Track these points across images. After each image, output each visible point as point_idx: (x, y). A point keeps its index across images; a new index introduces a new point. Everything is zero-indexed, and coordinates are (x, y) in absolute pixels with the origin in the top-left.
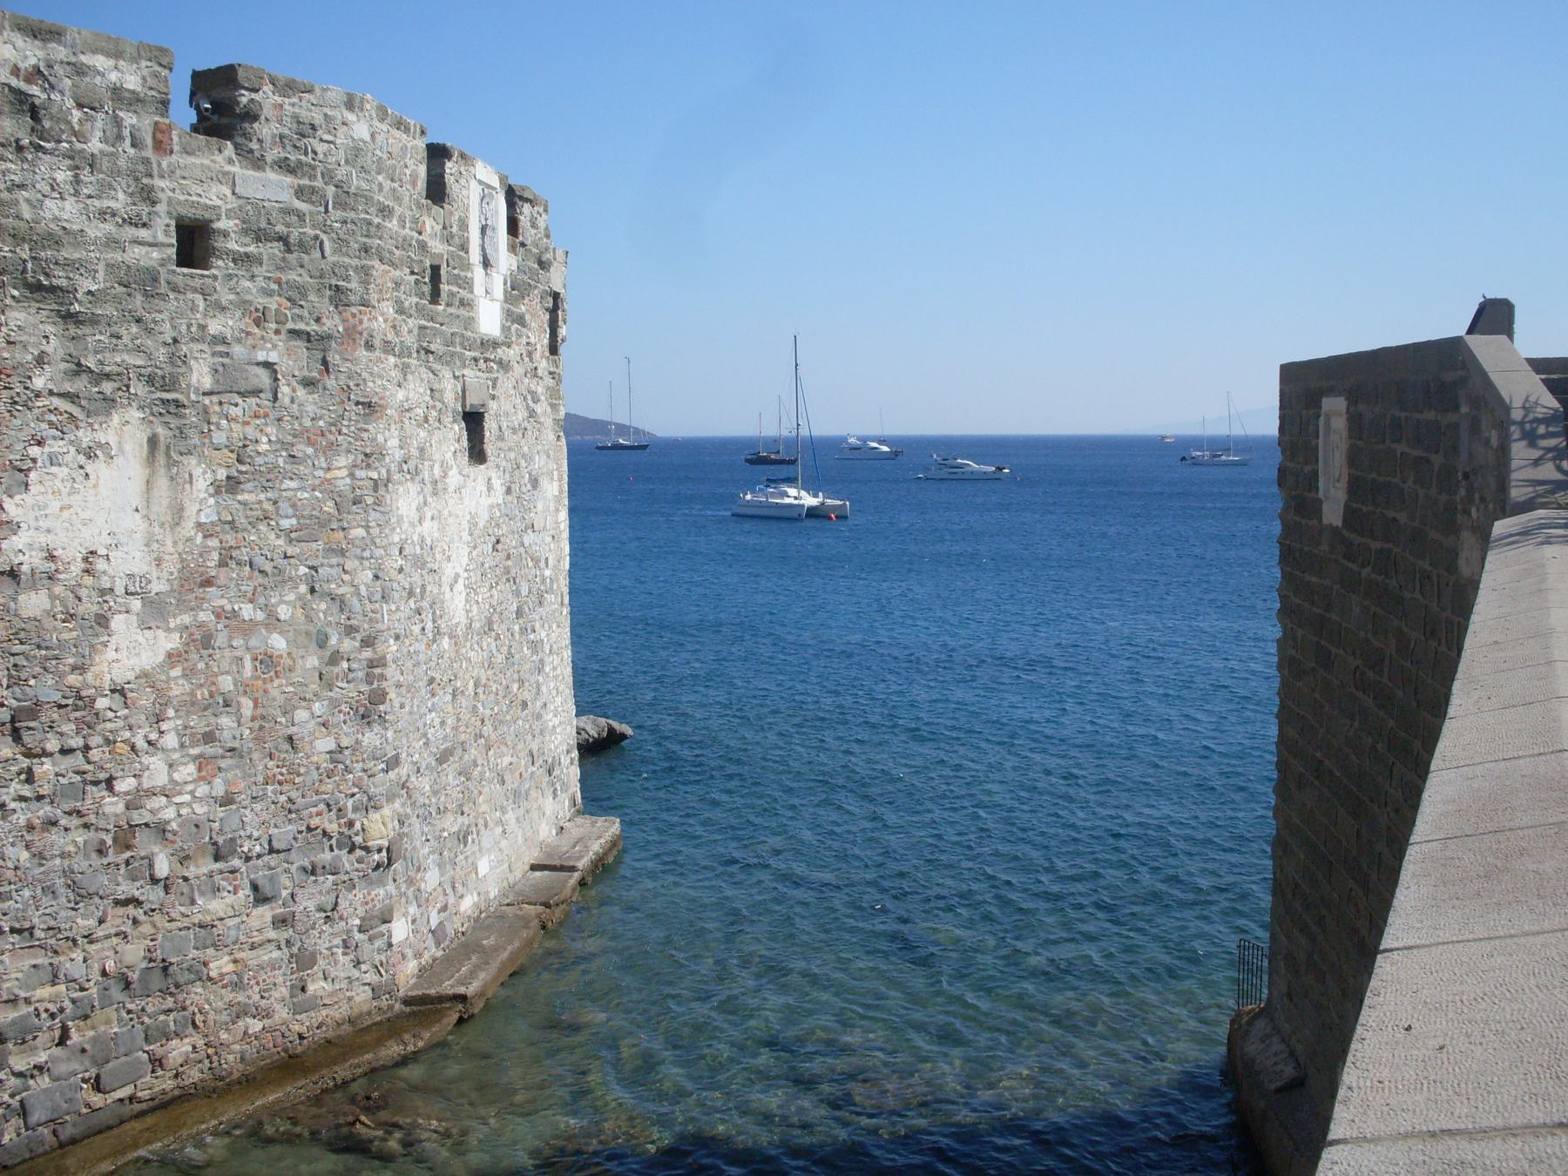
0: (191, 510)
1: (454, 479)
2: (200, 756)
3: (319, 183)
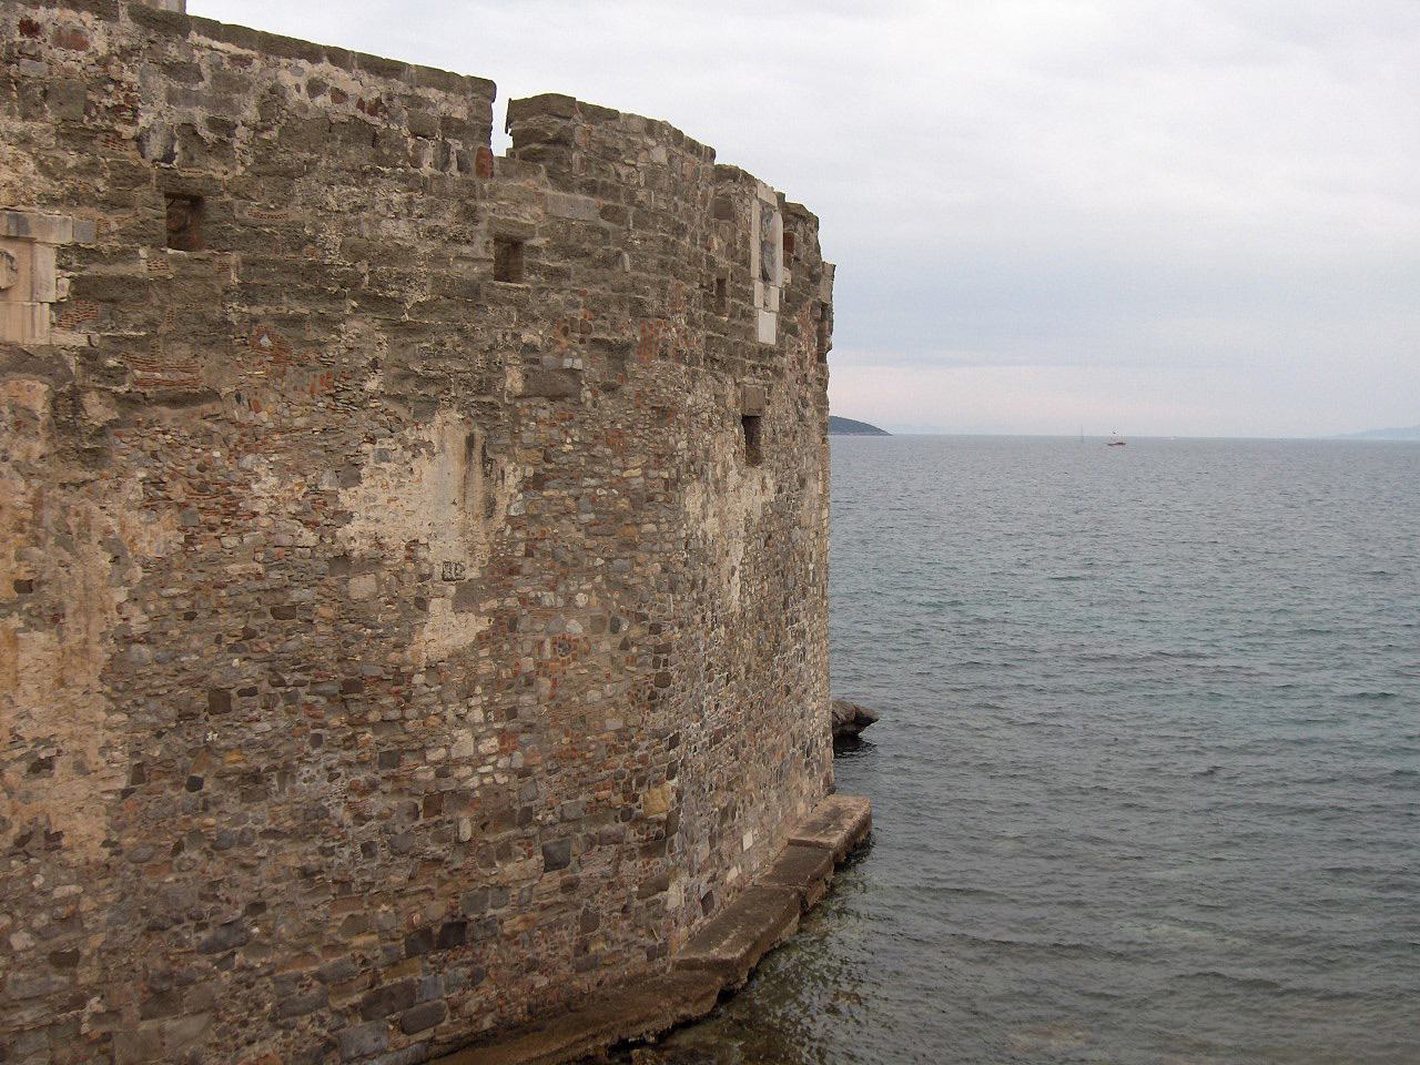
0: (502, 503)
1: (733, 478)
2: (503, 730)
3: (622, 204)
